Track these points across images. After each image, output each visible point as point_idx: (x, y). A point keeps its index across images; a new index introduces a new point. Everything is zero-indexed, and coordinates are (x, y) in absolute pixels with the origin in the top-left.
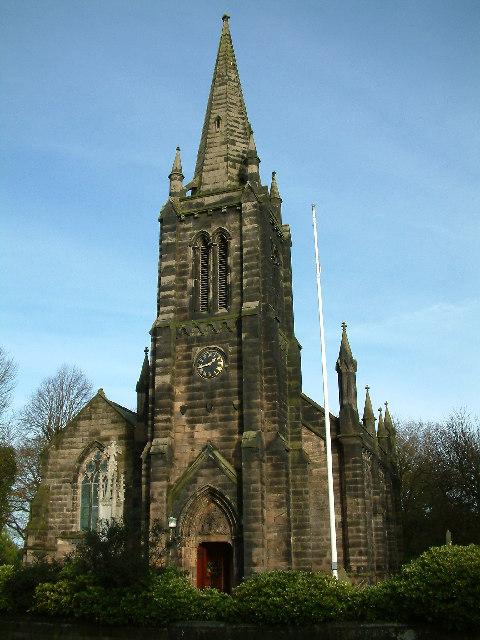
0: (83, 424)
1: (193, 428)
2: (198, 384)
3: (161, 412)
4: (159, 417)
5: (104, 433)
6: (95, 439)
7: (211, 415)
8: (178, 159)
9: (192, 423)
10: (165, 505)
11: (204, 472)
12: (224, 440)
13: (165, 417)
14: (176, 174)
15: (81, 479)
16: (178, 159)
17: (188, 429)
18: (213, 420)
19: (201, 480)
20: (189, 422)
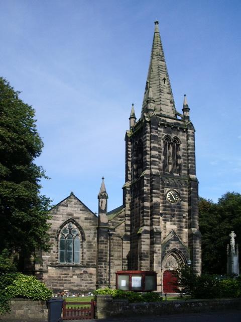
0: (61, 208)
1: (166, 223)
2: (167, 204)
3: (155, 214)
4: (155, 216)
5: (75, 215)
6: (70, 217)
7: (173, 219)
8: (103, 185)
9: (165, 221)
10: (15, 134)
11: (173, 242)
12: (179, 230)
13: (158, 217)
14: (133, 117)
15: (60, 236)
16: (103, 185)
17: (163, 223)
18: (174, 221)
19: (171, 245)
20: (163, 220)
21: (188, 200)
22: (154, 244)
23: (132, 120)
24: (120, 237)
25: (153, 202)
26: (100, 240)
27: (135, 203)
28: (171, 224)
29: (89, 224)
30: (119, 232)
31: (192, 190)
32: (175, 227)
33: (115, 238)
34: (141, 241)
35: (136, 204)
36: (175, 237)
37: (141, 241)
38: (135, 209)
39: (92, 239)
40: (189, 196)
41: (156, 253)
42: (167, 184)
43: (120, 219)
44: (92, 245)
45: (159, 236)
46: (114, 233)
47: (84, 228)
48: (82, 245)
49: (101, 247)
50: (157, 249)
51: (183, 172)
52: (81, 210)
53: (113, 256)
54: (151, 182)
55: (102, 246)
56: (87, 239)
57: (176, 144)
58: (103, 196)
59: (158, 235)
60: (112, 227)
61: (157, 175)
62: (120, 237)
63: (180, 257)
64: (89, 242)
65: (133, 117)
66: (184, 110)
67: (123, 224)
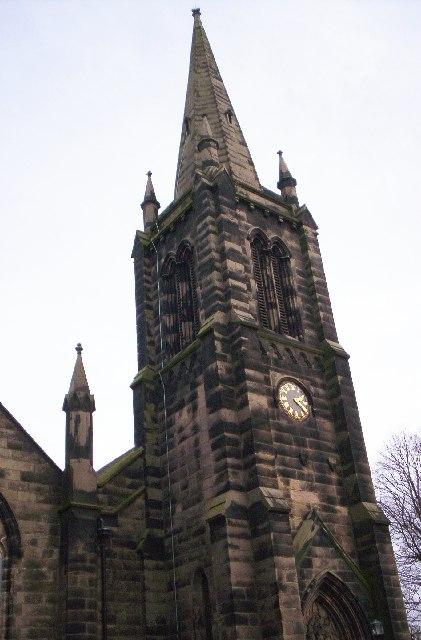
4: (261, 455)
7: (306, 471)
14: (150, 201)
19: (317, 562)
21: (335, 415)
22: (272, 555)
23: (150, 207)
24: (131, 545)
25: (250, 407)
26: (72, 553)
27: (176, 427)
28: (303, 489)
29: (33, 497)
30: (131, 528)
31: (342, 381)
32: (313, 499)
33: (117, 550)
34: (227, 546)
35: (181, 429)
36: (321, 532)
37: (227, 546)
38: (179, 447)
39: (44, 552)
40: (250, 457)
41: (284, 588)
42: (276, 360)
43: (129, 481)
44: (42, 575)
45: (281, 525)
46: (115, 529)
47: (17, 511)
48: (8, 576)
49: (75, 582)
50: (285, 573)
51: (306, 331)
52: (10, 446)
53: (113, 620)
54: (232, 347)
55: (79, 577)
56: (27, 550)
57: (279, 254)
58: (79, 403)
59: (280, 519)
60: (107, 509)
61: (247, 327)
62: (131, 545)
63: (344, 610)
64: (33, 564)
65: (150, 201)
66: (280, 186)
67: (141, 501)
